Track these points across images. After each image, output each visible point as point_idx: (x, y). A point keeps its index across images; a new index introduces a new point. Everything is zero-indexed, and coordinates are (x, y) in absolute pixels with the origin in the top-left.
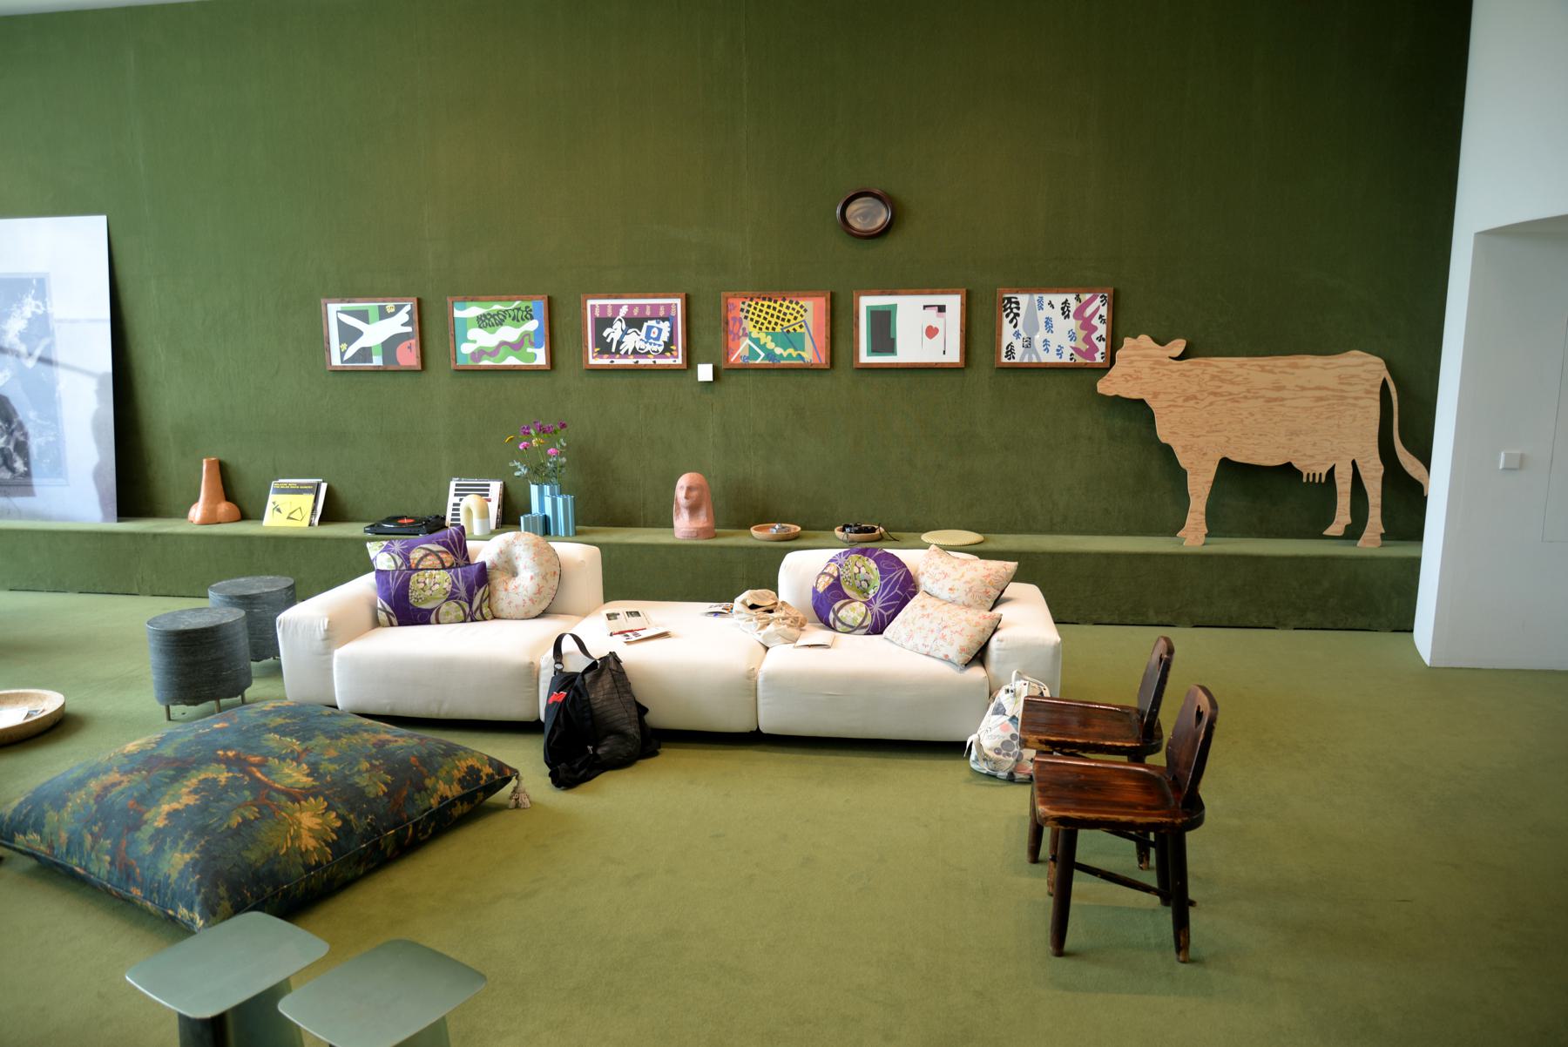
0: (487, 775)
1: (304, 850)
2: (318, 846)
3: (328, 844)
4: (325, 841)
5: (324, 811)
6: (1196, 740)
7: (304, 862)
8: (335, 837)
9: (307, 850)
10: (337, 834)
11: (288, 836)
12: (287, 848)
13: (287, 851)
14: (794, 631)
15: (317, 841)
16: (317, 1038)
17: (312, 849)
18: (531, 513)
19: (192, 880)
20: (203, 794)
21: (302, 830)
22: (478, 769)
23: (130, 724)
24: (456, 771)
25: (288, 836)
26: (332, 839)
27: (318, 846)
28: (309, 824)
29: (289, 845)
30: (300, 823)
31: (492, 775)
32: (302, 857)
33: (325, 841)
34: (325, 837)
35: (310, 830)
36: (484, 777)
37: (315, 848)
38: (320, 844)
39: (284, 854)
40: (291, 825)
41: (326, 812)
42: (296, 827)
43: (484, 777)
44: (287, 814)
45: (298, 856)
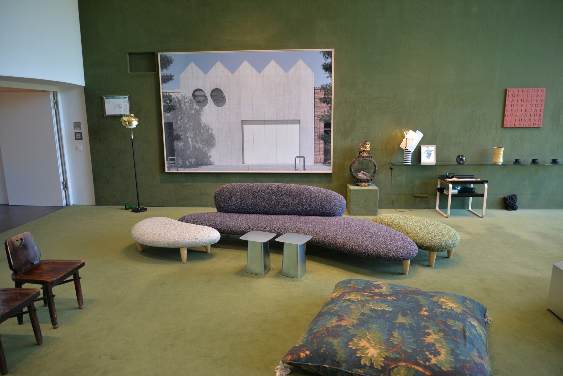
0: (431, 359)
1: (362, 339)
2: (359, 345)
3: (357, 350)
4: (358, 350)
5: (372, 361)
6: (197, 165)
7: (357, 336)
8: (358, 355)
9: (361, 340)
10: (358, 357)
11: (371, 339)
12: (368, 335)
13: (366, 334)
14: (119, 105)
15: (361, 346)
16: (436, 260)
17: (359, 342)
18: (379, 208)
19: (324, 349)
20: (427, 309)
21: (370, 345)
22: (437, 356)
23: (443, 351)
24: (440, 345)
25: (371, 339)
26: (357, 353)
27: (359, 345)
28: (370, 350)
29: (368, 337)
30: (374, 348)
31: (430, 362)
32: (359, 337)
33: (358, 350)
34: (360, 351)
35: (368, 348)
36: (430, 356)
37: (359, 343)
38: (359, 346)
39: (366, 333)
40: (376, 344)
41: (371, 362)
42: (373, 345)
43: (430, 356)
44: (382, 348)
45: (361, 336)
